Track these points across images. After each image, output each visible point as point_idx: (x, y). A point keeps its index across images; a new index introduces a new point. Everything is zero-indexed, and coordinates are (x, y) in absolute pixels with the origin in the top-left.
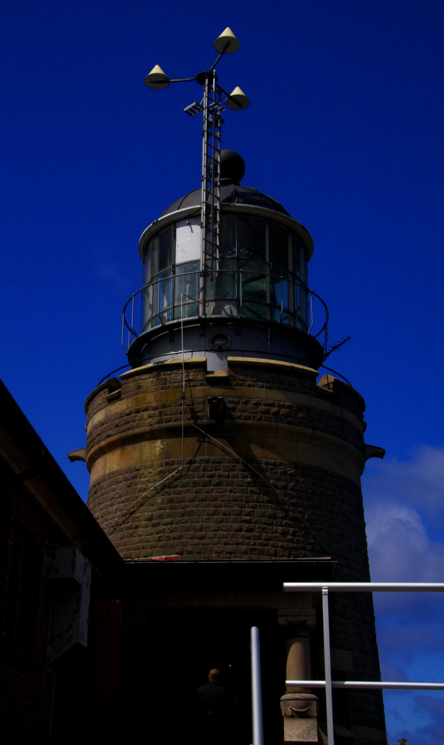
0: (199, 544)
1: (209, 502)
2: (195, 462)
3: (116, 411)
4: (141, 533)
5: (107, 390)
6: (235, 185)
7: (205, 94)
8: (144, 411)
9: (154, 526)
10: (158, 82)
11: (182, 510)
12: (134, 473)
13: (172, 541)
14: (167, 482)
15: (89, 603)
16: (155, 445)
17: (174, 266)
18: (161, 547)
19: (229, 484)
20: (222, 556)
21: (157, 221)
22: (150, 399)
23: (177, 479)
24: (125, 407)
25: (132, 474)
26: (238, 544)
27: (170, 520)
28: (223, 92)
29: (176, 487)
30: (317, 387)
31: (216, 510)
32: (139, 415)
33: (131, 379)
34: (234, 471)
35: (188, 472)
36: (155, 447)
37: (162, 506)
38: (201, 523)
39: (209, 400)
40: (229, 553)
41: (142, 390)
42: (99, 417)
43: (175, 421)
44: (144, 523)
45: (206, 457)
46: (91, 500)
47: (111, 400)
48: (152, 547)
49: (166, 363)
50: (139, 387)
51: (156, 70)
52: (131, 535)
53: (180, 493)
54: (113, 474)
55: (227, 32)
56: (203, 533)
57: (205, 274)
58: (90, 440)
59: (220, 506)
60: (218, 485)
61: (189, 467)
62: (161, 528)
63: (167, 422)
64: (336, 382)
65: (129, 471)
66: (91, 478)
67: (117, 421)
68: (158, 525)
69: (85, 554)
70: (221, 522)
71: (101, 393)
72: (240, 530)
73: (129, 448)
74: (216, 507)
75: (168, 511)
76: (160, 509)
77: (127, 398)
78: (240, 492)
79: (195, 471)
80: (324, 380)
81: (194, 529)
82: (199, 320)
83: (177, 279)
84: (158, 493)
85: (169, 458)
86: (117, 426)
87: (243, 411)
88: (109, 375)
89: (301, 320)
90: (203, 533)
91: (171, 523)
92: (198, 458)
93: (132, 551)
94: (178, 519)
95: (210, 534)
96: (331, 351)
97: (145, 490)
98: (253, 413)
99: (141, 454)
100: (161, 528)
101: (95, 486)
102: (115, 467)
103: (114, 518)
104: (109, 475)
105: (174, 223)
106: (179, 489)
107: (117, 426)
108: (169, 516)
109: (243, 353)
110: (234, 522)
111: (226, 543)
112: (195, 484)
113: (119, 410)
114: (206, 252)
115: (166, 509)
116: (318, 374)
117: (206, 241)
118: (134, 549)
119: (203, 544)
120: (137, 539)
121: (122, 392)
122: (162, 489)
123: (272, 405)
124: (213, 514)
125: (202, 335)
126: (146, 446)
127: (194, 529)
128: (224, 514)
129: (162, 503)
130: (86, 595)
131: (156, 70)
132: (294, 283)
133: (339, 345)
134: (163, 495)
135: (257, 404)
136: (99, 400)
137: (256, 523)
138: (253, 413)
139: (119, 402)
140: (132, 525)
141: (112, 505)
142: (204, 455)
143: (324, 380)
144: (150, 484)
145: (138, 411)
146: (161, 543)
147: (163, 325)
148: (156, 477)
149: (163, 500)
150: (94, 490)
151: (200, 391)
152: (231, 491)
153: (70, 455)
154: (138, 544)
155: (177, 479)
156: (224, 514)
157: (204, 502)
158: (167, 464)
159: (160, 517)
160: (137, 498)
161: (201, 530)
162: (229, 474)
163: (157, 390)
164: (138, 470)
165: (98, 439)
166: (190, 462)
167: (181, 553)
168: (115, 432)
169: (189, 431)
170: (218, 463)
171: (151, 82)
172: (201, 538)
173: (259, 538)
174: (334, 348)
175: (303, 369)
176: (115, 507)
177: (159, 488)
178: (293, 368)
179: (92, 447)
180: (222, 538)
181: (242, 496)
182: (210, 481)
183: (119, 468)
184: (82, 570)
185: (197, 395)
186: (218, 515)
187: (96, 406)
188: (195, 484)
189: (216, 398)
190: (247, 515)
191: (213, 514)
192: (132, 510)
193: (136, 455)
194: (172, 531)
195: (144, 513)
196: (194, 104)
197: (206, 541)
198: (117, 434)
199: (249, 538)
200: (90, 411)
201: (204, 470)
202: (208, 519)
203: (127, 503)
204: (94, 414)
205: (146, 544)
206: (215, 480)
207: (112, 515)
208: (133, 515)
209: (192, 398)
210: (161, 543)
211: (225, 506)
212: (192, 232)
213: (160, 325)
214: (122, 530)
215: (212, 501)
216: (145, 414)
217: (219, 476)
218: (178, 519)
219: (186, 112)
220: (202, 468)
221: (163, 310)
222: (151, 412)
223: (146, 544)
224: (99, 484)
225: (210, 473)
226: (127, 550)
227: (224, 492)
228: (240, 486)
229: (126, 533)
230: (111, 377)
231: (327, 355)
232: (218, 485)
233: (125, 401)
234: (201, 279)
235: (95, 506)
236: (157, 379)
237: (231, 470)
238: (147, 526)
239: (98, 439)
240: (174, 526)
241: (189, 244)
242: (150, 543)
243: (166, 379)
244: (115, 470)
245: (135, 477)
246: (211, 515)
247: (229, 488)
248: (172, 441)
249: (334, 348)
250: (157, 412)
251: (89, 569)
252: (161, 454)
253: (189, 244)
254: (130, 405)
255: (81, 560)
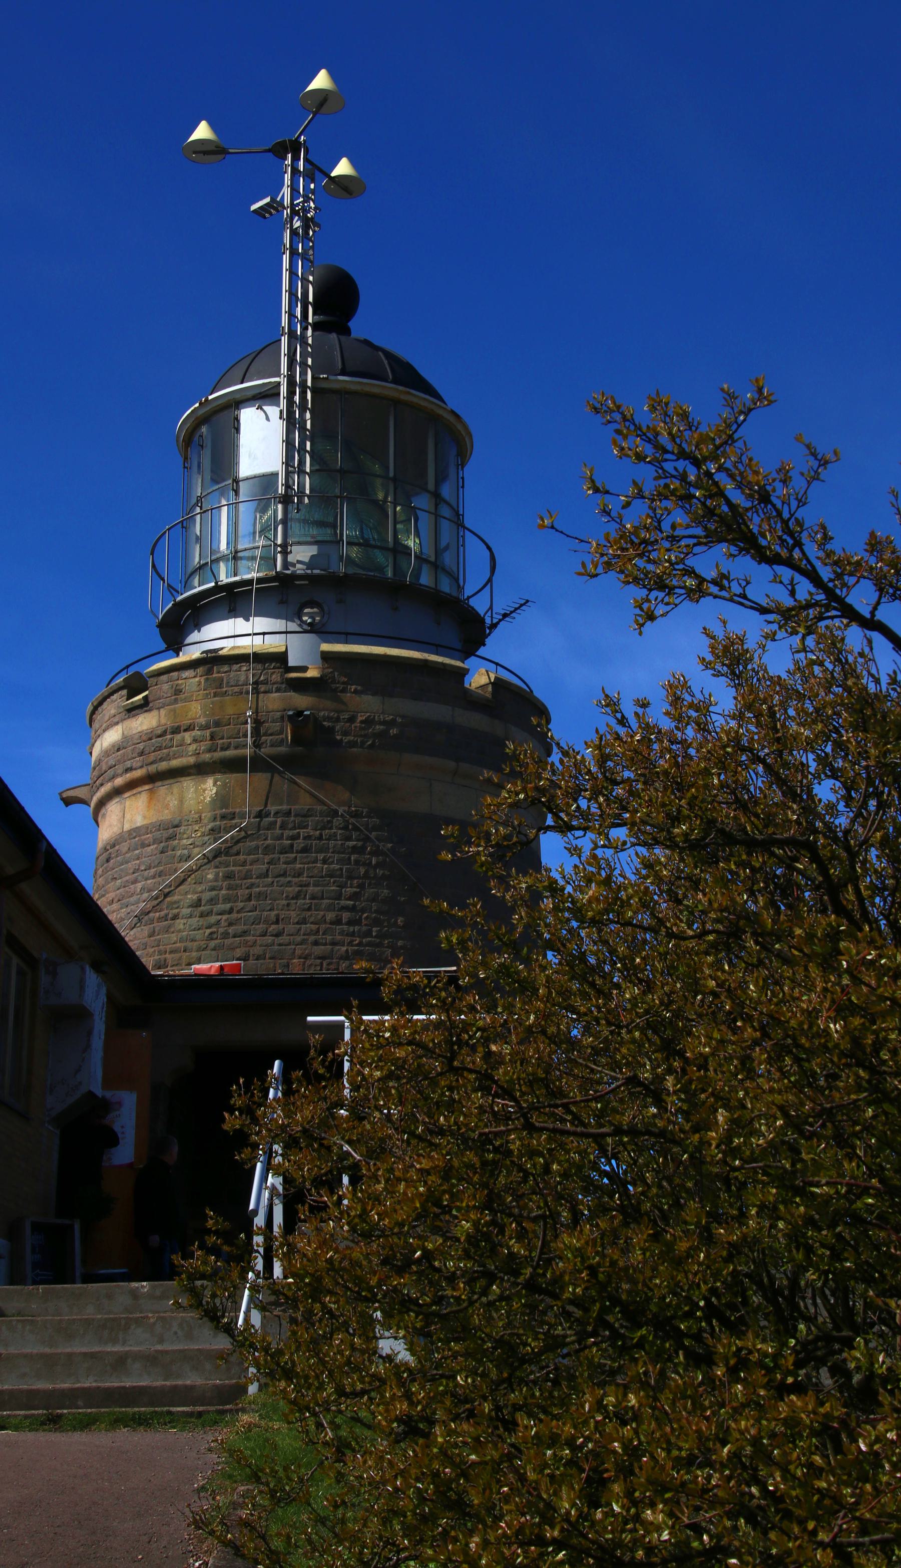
0: (273, 944)
1: (289, 879)
2: (268, 815)
3: (140, 729)
4: (182, 927)
5: (125, 692)
6: (338, 333)
7: (287, 177)
8: (185, 730)
9: (202, 915)
10: (205, 153)
11: (247, 891)
12: (171, 831)
13: (231, 940)
14: (223, 846)
15: (103, 1037)
16: (204, 787)
17: (236, 481)
18: (214, 949)
19: (320, 851)
20: (308, 962)
21: (207, 400)
22: (196, 710)
23: (238, 842)
24: (154, 723)
25: (167, 832)
26: (334, 944)
27: (228, 906)
28: (317, 170)
29: (238, 854)
30: (467, 692)
31: (299, 892)
32: (178, 737)
33: (164, 678)
34: (331, 828)
35: (259, 830)
36: (204, 790)
37: (215, 884)
38: (276, 912)
39: (289, 716)
40: (319, 958)
41: (183, 696)
42: (112, 737)
43: (236, 748)
44: (186, 911)
45: (285, 807)
46: (100, 872)
47: (132, 711)
48: (199, 949)
49: (221, 653)
50: (178, 691)
51: (202, 131)
52: (167, 930)
53: (244, 864)
54: (135, 832)
55: (321, 81)
56: (281, 926)
57: (286, 500)
58: (96, 773)
59: (308, 885)
60: (305, 850)
61: (260, 822)
62: (213, 919)
63: (223, 749)
64: (498, 684)
65: (161, 826)
66: (100, 836)
67: (141, 746)
68: (209, 913)
69: (97, 966)
70: (309, 909)
71: (115, 696)
72: (338, 922)
73: (162, 789)
74: (301, 886)
75: (224, 892)
76: (212, 889)
77: (159, 709)
78: (340, 861)
79: (268, 829)
80: (479, 678)
81: (266, 921)
82: (279, 577)
83: (242, 507)
84: (209, 862)
85: (227, 808)
86: (142, 754)
87: (346, 733)
88: (128, 667)
89: (449, 574)
90: (281, 926)
91: (231, 911)
92: (273, 809)
93: (167, 956)
94: (242, 904)
95: (290, 928)
96: (500, 620)
97: (189, 858)
98: (361, 736)
99: (181, 801)
100: (213, 919)
101: (106, 850)
102: (139, 821)
103: (137, 902)
104: (130, 832)
105: (238, 402)
106: (241, 857)
107: (142, 754)
108: (227, 899)
109: (346, 637)
110: (329, 908)
111: (316, 943)
112: (267, 850)
113: (145, 728)
114: (288, 461)
115: (221, 889)
116: (468, 670)
117: (289, 442)
118: (171, 952)
119: (280, 945)
120: (174, 937)
121: (150, 699)
122: (215, 857)
123: (392, 723)
124: (296, 897)
125: (282, 602)
126: (188, 785)
127: (266, 921)
128: (313, 897)
129: (216, 879)
130: (99, 1026)
131: (202, 131)
132: (437, 516)
133: (512, 612)
134: (217, 867)
135: (368, 722)
136: (110, 708)
137: (363, 911)
138: (361, 736)
139: (146, 714)
140: (167, 915)
141: (135, 881)
142: (281, 804)
143: (479, 678)
144: (196, 850)
145: (176, 730)
146: (212, 944)
147: (216, 583)
148: (206, 838)
149: (217, 875)
150: (105, 855)
151: (274, 701)
152: (325, 861)
153: (64, 795)
154: (176, 945)
155: (238, 842)
156: (313, 897)
157: (282, 879)
158: (223, 817)
159: (212, 901)
160: (176, 871)
161: (277, 922)
162: (321, 835)
163: (206, 696)
164: (177, 826)
165: (111, 772)
166: (260, 815)
167: (245, 958)
168: (139, 764)
169: (259, 764)
170: (305, 816)
171: (194, 153)
172: (277, 935)
173: (368, 933)
174: (505, 616)
175: (442, 664)
176: (139, 886)
177: (210, 856)
178: (426, 661)
179: (102, 785)
180: (308, 935)
181: (341, 869)
182: (292, 846)
183: (146, 822)
184: (94, 992)
185: (271, 707)
186: (305, 898)
187: (107, 718)
188: (267, 850)
189: (300, 713)
190: (349, 899)
191: (296, 897)
192: (167, 890)
193: (173, 803)
194: (230, 924)
195: (186, 896)
196: (268, 200)
197: (284, 939)
198: (141, 767)
199: (353, 934)
200: (96, 725)
201: (281, 827)
202: (288, 905)
203: (159, 879)
204: (104, 731)
205: (189, 944)
206: (299, 844)
207: (135, 898)
208: (168, 899)
209: (286, 632)
210: (212, 944)
211: (315, 885)
212: (268, 419)
213: (213, 584)
214: (152, 921)
215: (294, 877)
216: (188, 737)
217: (308, 837)
218: (242, 904)
219: (255, 211)
220: (278, 824)
221: (218, 555)
222: (197, 733)
223: (189, 944)
224: (114, 846)
225: (291, 833)
226: (160, 953)
227: (314, 862)
228: (339, 853)
229: (158, 926)
230: (131, 671)
231: (494, 626)
232: (305, 850)
233: (155, 713)
234: (280, 506)
235: (107, 883)
236: (207, 679)
237: (323, 828)
238: (191, 917)
239: (111, 772)
240: (234, 916)
241: (261, 441)
242: (195, 944)
243: (222, 679)
244: (139, 824)
245: (172, 837)
246: (293, 898)
247: (321, 856)
248: (232, 778)
249: (505, 616)
250: (207, 733)
251: (104, 991)
252: (213, 801)
253: (261, 441)
254: (163, 721)
255: (92, 978)
